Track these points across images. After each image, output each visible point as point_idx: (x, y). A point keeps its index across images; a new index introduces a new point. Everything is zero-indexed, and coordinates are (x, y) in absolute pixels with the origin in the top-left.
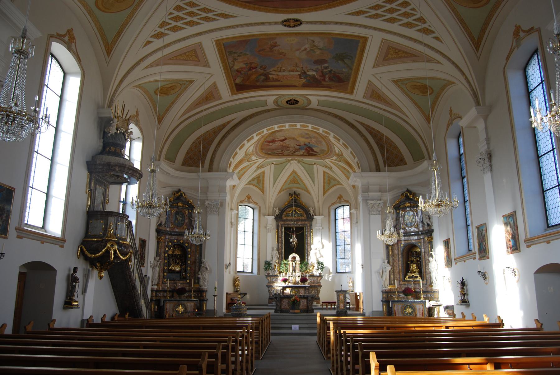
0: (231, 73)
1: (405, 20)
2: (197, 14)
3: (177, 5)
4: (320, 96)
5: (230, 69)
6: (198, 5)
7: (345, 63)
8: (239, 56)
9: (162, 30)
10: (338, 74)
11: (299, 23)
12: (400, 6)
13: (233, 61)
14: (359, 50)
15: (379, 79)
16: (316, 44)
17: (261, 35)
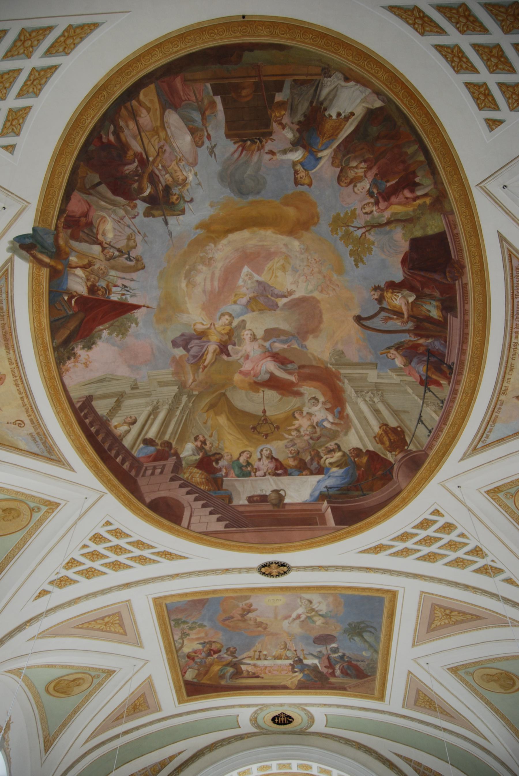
0: (179, 660)
1: (453, 556)
2: (126, 551)
3: (97, 532)
4: (330, 706)
5: (177, 652)
6: (128, 536)
7: (366, 641)
8: (191, 629)
9: (70, 574)
10: (216, 283)
11: (285, 569)
12: (440, 532)
13: (181, 638)
14: (385, 614)
15: (426, 666)
16: (315, 606)
17: (227, 590)
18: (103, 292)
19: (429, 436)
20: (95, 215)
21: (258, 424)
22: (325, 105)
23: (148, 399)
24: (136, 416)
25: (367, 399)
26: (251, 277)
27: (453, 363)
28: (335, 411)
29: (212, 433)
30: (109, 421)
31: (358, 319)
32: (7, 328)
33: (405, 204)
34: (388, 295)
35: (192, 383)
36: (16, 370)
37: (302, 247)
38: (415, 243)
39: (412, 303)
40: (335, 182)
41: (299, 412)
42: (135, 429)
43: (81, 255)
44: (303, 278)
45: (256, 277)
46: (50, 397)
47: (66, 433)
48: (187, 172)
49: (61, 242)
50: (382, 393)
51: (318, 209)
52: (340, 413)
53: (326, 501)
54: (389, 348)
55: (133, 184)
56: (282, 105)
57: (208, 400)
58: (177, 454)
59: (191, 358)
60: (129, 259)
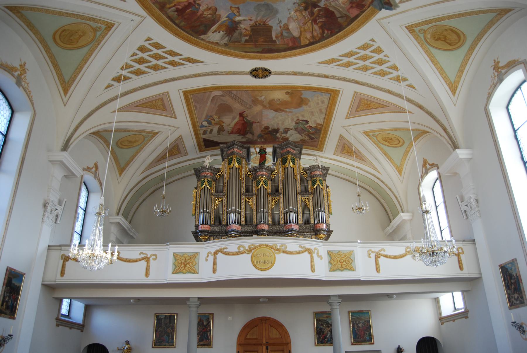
22: (226, 35)
48: (294, 15)
55: (323, 14)
56: (245, 36)
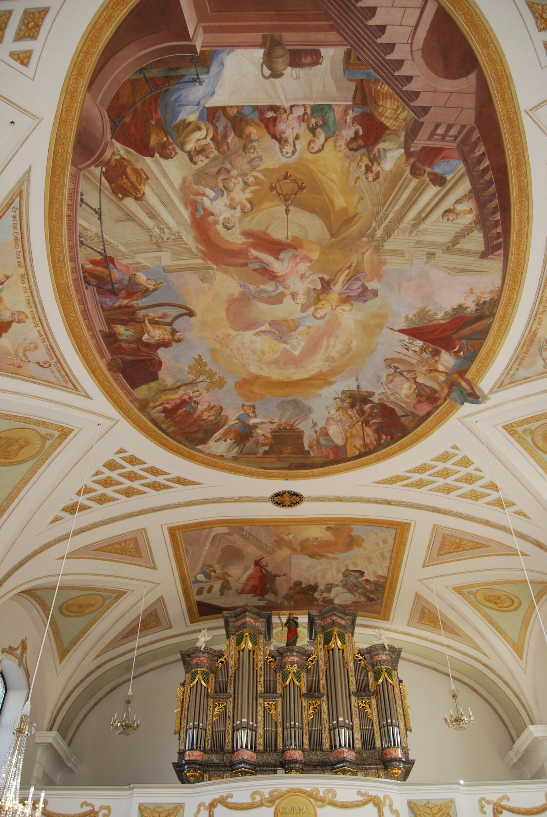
10: (325, 343)
18: (428, 349)
19: (82, 195)
20: (413, 400)
21: (295, 194)
22: (235, 445)
23: (421, 238)
24: (441, 220)
25: (166, 231)
26: (293, 347)
27: (87, 288)
28: (202, 212)
29: (355, 183)
30: (475, 222)
31: (191, 314)
32: (525, 349)
33: (169, 400)
34: (167, 337)
35: (367, 251)
36: (540, 311)
37: (248, 368)
38: (154, 377)
39: (144, 334)
40: (224, 406)
41: (246, 211)
42: (447, 204)
43: (435, 380)
44: (246, 345)
45: (288, 347)
46: (524, 272)
47: (530, 224)
49: (446, 391)
50: (152, 240)
51: (236, 391)
52: (196, 210)
53: (199, 49)
54: (155, 290)
56: (264, 445)
57: (352, 230)
58: (408, 154)
59: (362, 278)
60: (396, 368)
